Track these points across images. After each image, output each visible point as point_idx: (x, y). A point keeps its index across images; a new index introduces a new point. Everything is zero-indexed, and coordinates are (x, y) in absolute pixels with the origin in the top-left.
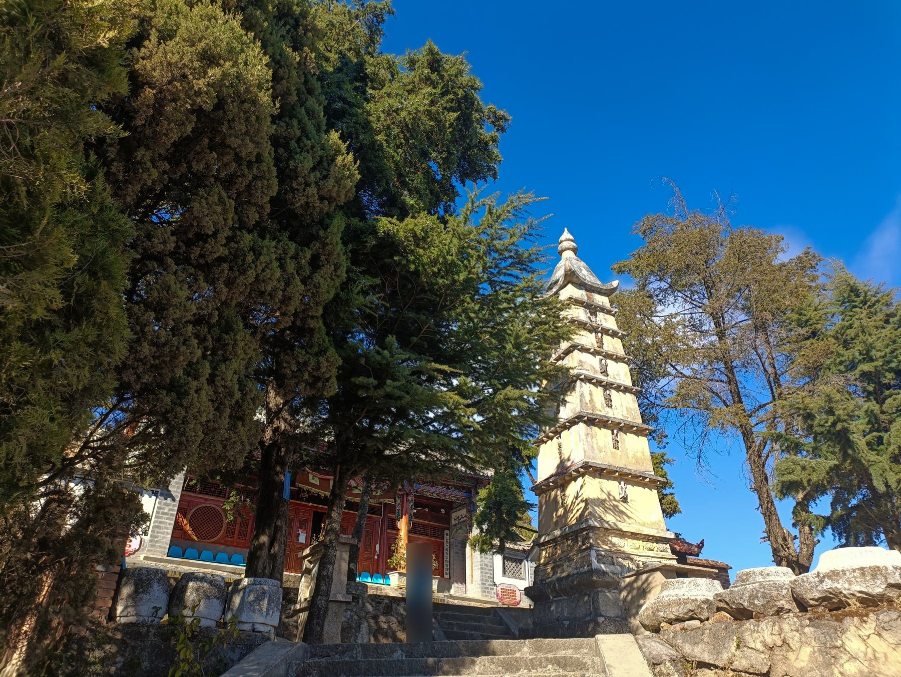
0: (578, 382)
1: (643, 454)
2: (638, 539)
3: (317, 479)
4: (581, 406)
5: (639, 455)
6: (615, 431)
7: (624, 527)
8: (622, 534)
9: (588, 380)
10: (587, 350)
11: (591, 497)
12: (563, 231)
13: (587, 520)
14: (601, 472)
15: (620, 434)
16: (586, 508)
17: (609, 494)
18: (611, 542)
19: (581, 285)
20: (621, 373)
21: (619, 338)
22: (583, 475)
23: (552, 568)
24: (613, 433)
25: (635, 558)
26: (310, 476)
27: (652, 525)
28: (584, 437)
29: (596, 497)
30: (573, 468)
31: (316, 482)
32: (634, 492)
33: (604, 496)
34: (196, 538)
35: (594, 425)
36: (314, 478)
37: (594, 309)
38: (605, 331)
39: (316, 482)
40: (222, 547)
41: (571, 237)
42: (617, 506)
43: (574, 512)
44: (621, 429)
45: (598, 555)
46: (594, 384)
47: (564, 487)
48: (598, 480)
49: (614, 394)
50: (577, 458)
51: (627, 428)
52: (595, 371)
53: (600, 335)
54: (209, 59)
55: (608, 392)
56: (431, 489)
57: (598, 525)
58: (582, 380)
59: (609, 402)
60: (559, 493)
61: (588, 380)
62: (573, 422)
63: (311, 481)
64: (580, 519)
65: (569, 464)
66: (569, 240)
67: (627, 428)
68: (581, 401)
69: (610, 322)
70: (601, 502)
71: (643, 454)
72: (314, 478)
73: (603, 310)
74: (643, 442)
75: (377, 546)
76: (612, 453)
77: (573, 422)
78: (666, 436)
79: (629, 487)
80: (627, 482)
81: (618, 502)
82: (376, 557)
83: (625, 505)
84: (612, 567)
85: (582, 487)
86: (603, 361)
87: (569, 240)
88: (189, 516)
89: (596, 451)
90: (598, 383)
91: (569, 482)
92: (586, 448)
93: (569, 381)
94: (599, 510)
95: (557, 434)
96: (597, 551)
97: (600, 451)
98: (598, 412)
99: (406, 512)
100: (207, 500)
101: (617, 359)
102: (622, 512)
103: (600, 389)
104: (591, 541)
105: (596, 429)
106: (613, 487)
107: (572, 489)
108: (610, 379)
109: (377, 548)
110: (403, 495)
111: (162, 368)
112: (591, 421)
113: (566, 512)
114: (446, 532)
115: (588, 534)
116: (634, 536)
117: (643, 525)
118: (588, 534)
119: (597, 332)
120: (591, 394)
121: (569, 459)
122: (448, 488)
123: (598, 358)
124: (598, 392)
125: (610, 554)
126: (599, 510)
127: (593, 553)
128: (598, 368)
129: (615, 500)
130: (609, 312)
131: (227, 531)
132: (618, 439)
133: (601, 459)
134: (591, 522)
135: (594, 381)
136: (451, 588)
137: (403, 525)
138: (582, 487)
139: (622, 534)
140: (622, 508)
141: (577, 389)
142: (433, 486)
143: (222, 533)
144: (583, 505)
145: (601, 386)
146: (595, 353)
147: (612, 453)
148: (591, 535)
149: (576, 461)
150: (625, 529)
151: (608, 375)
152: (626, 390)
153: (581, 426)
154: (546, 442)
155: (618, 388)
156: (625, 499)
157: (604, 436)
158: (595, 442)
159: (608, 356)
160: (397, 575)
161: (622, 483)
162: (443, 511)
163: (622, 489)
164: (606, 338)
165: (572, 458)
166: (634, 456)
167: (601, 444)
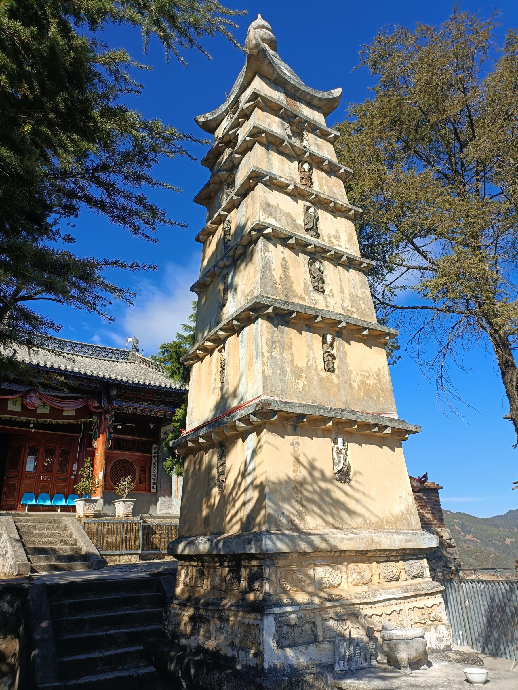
0: (261, 241)
1: (379, 379)
2: (369, 560)
4: (263, 287)
5: (371, 382)
6: (329, 338)
7: (344, 541)
8: (336, 557)
9: (281, 239)
10: (282, 188)
11: (273, 478)
12: (256, 18)
13: (258, 537)
14: (294, 422)
15: (339, 342)
16: (259, 505)
17: (312, 468)
18: (312, 580)
19: (277, 82)
20: (340, 234)
21: (340, 177)
22: (258, 430)
23: (192, 618)
24: (324, 342)
25: (367, 611)
27: (395, 523)
28: (265, 349)
29: (283, 477)
30: (239, 414)
32: (362, 457)
33: (303, 473)
35: (287, 324)
37: (299, 126)
38: (317, 162)
41: (267, 24)
42: (327, 492)
43: (238, 504)
44: (339, 334)
45: (279, 626)
46: (291, 248)
47: (224, 448)
48: (289, 438)
49: (329, 270)
50: (251, 390)
51: (351, 332)
52: (297, 226)
53: (306, 166)
55: (317, 265)
56: (134, 405)
57: (283, 547)
58: (268, 238)
59: (319, 283)
60: (215, 459)
61: (281, 239)
62: (245, 319)
64: (248, 523)
65: (234, 404)
66: (263, 27)
67: (351, 332)
68: (263, 277)
69: (327, 151)
70: (294, 489)
71: (379, 379)
73: (314, 129)
74: (376, 359)
76: (321, 379)
77: (245, 319)
78: (398, 348)
79: (353, 447)
80: (349, 437)
81: (330, 481)
82: (73, 477)
83: (346, 487)
84: (312, 648)
85: (254, 453)
86: (312, 210)
87: (263, 27)
89: (289, 377)
90: (300, 247)
91: (233, 442)
92: (269, 371)
93: (245, 242)
94: (290, 509)
95: (219, 342)
96: (277, 617)
97: (298, 377)
98: (296, 300)
99: (105, 431)
101: (336, 211)
102: (338, 504)
103: (304, 259)
104: (267, 587)
105: (291, 333)
106: (320, 451)
107: (239, 454)
108: (323, 242)
110: (101, 413)
112: (282, 317)
113: (226, 500)
114: (154, 446)
115: (260, 567)
116: (363, 556)
117: (379, 527)
118: (260, 567)
119: (301, 162)
120: (284, 265)
121: (235, 395)
122: (154, 404)
123: (302, 204)
124: (300, 266)
125: (309, 615)
126: (290, 509)
127: (269, 623)
128: (300, 221)
129: (324, 478)
130: (324, 135)
132: (334, 352)
133: (297, 395)
134: (268, 544)
135: (292, 241)
136: (157, 501)
137: (100, 445)
138: (254, 453)
139: (336, 557)
140: (338, 494)
141: (257, 257)
142: (137, 402)
144: (255, 495)
145: (305, 253)
146: (297, 195)
147: (321, 379)
148: (267, 571)
149: (249, 397)
150: (343, 546)
151: (318, 236)
152: (350, 264)
153: (261, 327)
154: (202, 359)
155: (337, 259)
156: (344, 475)
157: (306, 347)
158: (288, 357)
159: (321, 203)
160: (82, 502)
161: (340, 440)
162: (152, 426)
163: (339, 452)
164: (317, 175)
165: (241, 391)
166: (363, 384)
167: (301, 363)
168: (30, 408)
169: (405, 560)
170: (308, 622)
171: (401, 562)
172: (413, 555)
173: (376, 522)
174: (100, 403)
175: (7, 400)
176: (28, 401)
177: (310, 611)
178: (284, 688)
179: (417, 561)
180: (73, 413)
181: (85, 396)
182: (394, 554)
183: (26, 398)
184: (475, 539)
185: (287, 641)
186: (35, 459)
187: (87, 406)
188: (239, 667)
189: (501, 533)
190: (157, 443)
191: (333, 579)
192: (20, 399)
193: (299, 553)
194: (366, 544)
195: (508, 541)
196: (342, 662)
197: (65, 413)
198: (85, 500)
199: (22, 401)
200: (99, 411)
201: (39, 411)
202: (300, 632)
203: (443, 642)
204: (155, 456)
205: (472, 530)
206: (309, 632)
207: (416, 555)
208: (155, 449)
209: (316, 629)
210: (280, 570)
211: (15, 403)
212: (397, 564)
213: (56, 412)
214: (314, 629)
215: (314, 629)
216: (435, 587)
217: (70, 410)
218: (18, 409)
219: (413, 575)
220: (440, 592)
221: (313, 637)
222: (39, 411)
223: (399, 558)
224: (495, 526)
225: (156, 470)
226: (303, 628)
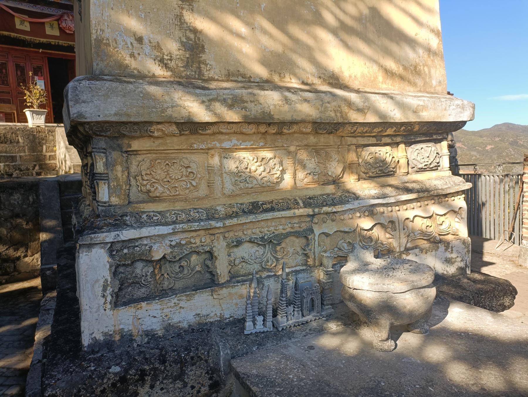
3: (28, 24)
26: (17, 21)
31: (27, 27)
36: (22, 22)
39: (27, 27)
72: (22, 22)
168: (67, 31)
169: (409, 144)
170: (198, 253)
171: (402, 146)
172: (424, 134)
173: (363, 76)
175: (43, 24)
177: (202, 233)
178: (103, 391)
179: (430, 144)
182: (389, 131)
183: (62, 22)
184: (463, 146)
185: (143, 290)
189: (484, 141)
191: (264, 174)
192: (56, 22)
193: (177, 124)
194: (335, 111)
195: (489, 147)
196: (260, 319)
199: (59, 25)
202: (178, 270)
203: (456, 264)
205: (462, 140)
206: (198, 268)
207: (431, 135)
209: (213, 264)
210: (139, 158)
211: (52, 26)
212: (395, 150)
214: (209, 263)
215: (209, 263)
216: (456, 185)
218: (57, 33)
219: (420, 166)
220: (463, 192)
221: (208, 276)
223: (399, 139)
224: (481, 137)
226: (184, 263)
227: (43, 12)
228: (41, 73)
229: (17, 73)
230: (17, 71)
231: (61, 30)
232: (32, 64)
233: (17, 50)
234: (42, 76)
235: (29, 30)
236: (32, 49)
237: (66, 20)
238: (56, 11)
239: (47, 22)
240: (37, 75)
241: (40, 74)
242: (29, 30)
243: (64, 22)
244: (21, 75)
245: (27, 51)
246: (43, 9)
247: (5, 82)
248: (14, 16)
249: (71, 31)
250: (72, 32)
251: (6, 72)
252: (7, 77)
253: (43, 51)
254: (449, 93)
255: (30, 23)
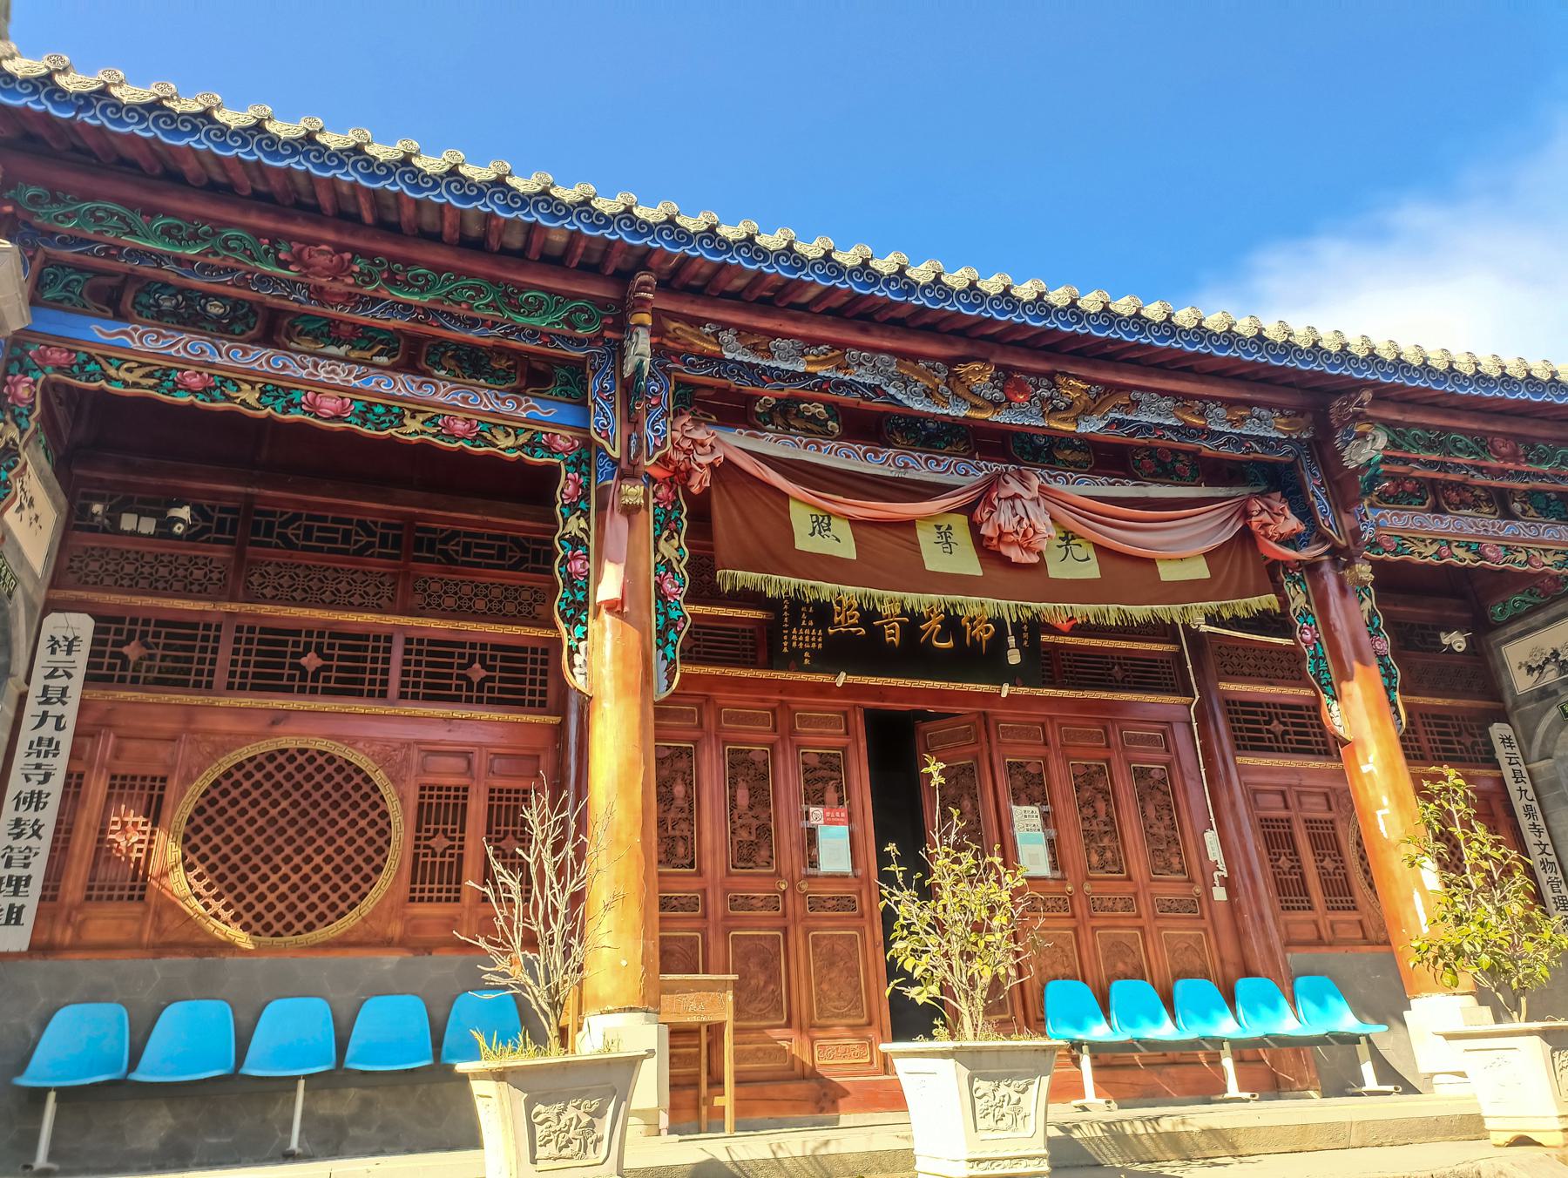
3: (842, 529)
26: (800, 518)
31: (841, 544)
34: (243, 939)
36: (822, 522)
39: (841, 544)
40: (390, 960)
54: (563, 1032)
63: (805, 541)
72: (822, 522)
75: (1211, 838)
82: (1220, 894)
88: (182, 808)
100: (279, 718)
109: (1214, 852)
111: (504, 946)
114: (1498, 730)
122: (1508, 515)
131: (418, 869)
143: (384, 881)
168: (1015, 554)
174: (1305, 513)
175: (909, 525)
176: (1005, 518)
180: (1200, 571)
181: (1233, 491)
186: (1045, 817)
187: (1246, 537)
188: (624, 963)
190: (1503, 717)
192: (963, 519)
197: (1168, 573)
198: (1545, 1034)
199: (974, 527)
200: (1306, 554)
201: (1055, 571)
204: (1517, 777)
208: (1505, 740)
211: (945, 535)
213: (1128, 570)
217: (1184, 548)
218: (967, 563)
222: (1055, 571)
225: (1545, 839)
227: (910, 475)
228: (838, 788)
229: (733, 798)
230: (733, 785)
231: (986, 550)
232: (799, 747)
233: (740, 683)
234: (840, 802)
235: (852, 554)
236: (803, 677)
237: (1017, 496)
238: (962, 467)
239: (928, 518)
240: (821, 802)
241: (831, 795)
242: (852, 554)
243: (1005, 506)
244: (751, 807)
245: (785, 687)
246: (906, 466)
247: (681, 850)
248: (786, 497)
249: (1028, 549)
250: (1035, 559)
251: (688, 796)
252: (689, 821)
253: (857, 680)
254: (1463, 1074)
255: (854, 522)
